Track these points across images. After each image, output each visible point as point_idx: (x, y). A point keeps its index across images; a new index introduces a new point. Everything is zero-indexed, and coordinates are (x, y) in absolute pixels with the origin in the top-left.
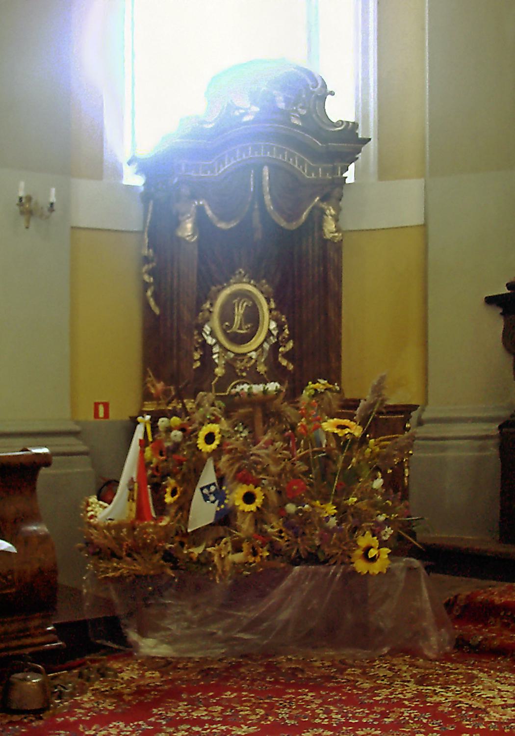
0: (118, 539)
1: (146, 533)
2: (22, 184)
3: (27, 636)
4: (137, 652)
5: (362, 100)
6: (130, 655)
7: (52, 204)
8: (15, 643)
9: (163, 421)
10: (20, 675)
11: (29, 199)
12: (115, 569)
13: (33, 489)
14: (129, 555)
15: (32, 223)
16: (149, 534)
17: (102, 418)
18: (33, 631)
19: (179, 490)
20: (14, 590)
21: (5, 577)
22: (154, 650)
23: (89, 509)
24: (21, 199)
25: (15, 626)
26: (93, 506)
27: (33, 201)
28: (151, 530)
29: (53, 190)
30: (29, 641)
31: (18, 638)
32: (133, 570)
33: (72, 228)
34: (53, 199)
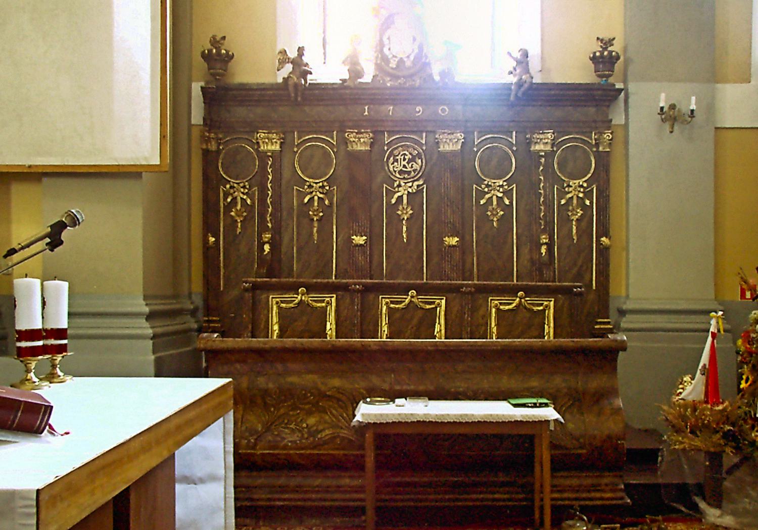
0: (683, 418)
1: (704, 415)
2: (663, 96)
3: (598, 491)
4: (704, 518)
5: (161, 300)
6: (700, 521)
7: (692, 111)
8: (584, 495)
9: (755, 314)
10: (570, 522)
11: (672, 107)
12: (681, 443)
13: (615, 369)
14: (692, 432)
15: (676, 128)
16: (706, 416)
17: (749, 299)
18: (603, 487)
19: (751, 379)
20: (584, 451)
21: (577, 440)
22: (719, 520)
23: (681, 386)
24: (662, 108)
25: (589, 481)
26: (686, 384)
27: (678, 107)
28: (708, 413)
29: (693, 98)
30: (598, 495)
31: (589, 491)
32: (694, 445)
33: (716, 128)
34: (693, 107)
